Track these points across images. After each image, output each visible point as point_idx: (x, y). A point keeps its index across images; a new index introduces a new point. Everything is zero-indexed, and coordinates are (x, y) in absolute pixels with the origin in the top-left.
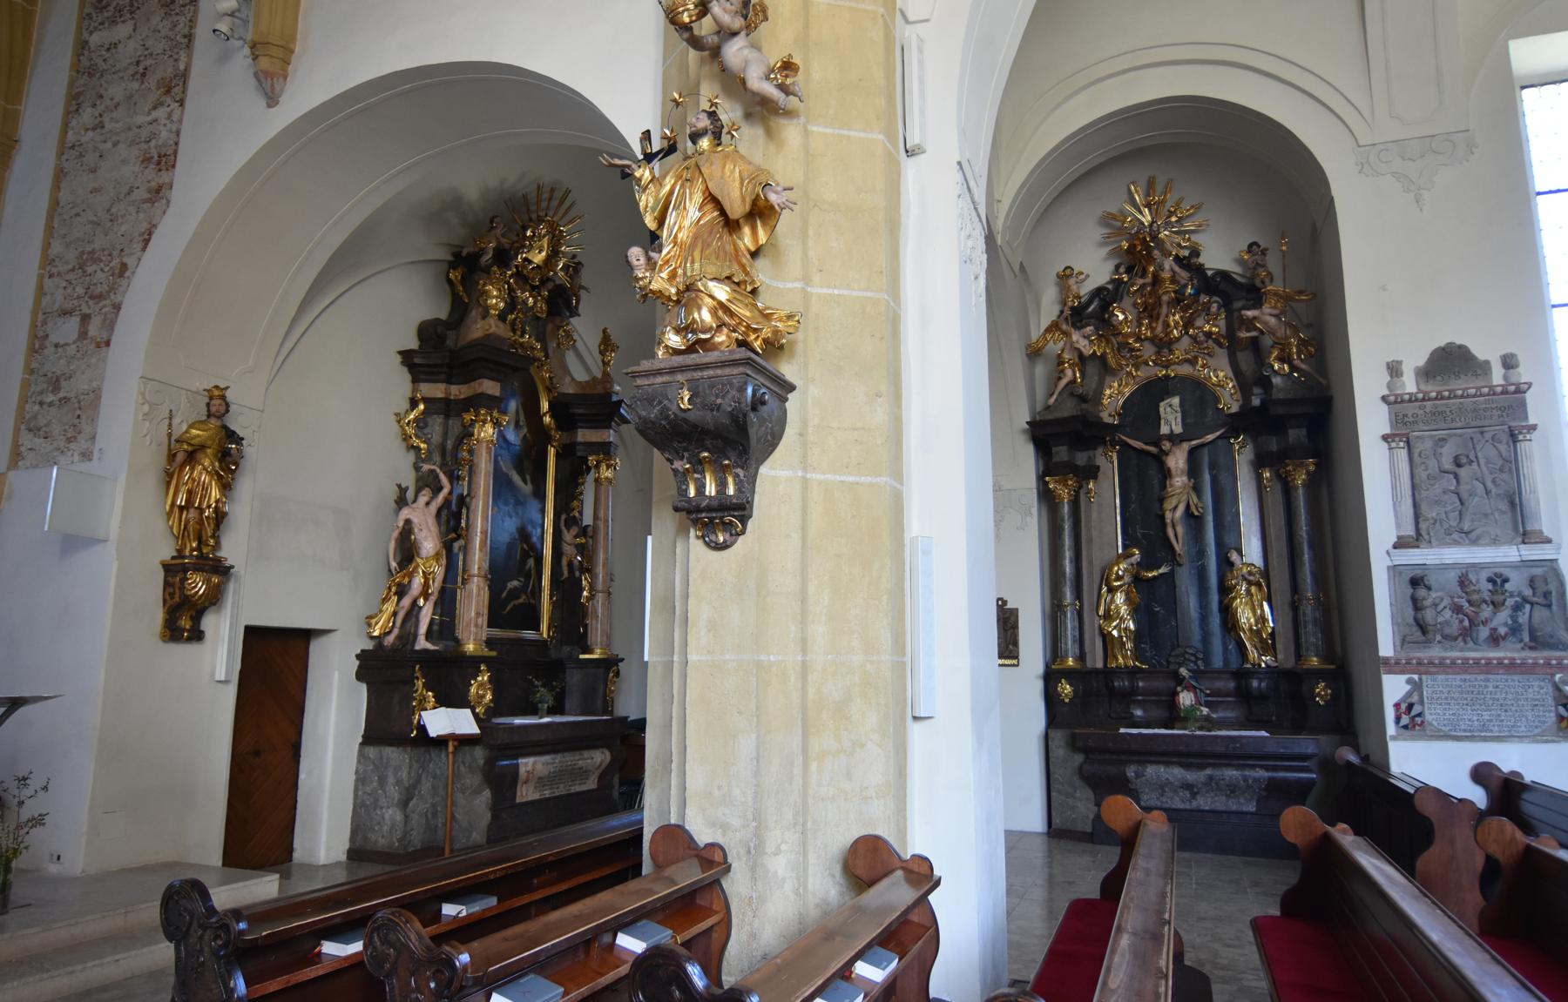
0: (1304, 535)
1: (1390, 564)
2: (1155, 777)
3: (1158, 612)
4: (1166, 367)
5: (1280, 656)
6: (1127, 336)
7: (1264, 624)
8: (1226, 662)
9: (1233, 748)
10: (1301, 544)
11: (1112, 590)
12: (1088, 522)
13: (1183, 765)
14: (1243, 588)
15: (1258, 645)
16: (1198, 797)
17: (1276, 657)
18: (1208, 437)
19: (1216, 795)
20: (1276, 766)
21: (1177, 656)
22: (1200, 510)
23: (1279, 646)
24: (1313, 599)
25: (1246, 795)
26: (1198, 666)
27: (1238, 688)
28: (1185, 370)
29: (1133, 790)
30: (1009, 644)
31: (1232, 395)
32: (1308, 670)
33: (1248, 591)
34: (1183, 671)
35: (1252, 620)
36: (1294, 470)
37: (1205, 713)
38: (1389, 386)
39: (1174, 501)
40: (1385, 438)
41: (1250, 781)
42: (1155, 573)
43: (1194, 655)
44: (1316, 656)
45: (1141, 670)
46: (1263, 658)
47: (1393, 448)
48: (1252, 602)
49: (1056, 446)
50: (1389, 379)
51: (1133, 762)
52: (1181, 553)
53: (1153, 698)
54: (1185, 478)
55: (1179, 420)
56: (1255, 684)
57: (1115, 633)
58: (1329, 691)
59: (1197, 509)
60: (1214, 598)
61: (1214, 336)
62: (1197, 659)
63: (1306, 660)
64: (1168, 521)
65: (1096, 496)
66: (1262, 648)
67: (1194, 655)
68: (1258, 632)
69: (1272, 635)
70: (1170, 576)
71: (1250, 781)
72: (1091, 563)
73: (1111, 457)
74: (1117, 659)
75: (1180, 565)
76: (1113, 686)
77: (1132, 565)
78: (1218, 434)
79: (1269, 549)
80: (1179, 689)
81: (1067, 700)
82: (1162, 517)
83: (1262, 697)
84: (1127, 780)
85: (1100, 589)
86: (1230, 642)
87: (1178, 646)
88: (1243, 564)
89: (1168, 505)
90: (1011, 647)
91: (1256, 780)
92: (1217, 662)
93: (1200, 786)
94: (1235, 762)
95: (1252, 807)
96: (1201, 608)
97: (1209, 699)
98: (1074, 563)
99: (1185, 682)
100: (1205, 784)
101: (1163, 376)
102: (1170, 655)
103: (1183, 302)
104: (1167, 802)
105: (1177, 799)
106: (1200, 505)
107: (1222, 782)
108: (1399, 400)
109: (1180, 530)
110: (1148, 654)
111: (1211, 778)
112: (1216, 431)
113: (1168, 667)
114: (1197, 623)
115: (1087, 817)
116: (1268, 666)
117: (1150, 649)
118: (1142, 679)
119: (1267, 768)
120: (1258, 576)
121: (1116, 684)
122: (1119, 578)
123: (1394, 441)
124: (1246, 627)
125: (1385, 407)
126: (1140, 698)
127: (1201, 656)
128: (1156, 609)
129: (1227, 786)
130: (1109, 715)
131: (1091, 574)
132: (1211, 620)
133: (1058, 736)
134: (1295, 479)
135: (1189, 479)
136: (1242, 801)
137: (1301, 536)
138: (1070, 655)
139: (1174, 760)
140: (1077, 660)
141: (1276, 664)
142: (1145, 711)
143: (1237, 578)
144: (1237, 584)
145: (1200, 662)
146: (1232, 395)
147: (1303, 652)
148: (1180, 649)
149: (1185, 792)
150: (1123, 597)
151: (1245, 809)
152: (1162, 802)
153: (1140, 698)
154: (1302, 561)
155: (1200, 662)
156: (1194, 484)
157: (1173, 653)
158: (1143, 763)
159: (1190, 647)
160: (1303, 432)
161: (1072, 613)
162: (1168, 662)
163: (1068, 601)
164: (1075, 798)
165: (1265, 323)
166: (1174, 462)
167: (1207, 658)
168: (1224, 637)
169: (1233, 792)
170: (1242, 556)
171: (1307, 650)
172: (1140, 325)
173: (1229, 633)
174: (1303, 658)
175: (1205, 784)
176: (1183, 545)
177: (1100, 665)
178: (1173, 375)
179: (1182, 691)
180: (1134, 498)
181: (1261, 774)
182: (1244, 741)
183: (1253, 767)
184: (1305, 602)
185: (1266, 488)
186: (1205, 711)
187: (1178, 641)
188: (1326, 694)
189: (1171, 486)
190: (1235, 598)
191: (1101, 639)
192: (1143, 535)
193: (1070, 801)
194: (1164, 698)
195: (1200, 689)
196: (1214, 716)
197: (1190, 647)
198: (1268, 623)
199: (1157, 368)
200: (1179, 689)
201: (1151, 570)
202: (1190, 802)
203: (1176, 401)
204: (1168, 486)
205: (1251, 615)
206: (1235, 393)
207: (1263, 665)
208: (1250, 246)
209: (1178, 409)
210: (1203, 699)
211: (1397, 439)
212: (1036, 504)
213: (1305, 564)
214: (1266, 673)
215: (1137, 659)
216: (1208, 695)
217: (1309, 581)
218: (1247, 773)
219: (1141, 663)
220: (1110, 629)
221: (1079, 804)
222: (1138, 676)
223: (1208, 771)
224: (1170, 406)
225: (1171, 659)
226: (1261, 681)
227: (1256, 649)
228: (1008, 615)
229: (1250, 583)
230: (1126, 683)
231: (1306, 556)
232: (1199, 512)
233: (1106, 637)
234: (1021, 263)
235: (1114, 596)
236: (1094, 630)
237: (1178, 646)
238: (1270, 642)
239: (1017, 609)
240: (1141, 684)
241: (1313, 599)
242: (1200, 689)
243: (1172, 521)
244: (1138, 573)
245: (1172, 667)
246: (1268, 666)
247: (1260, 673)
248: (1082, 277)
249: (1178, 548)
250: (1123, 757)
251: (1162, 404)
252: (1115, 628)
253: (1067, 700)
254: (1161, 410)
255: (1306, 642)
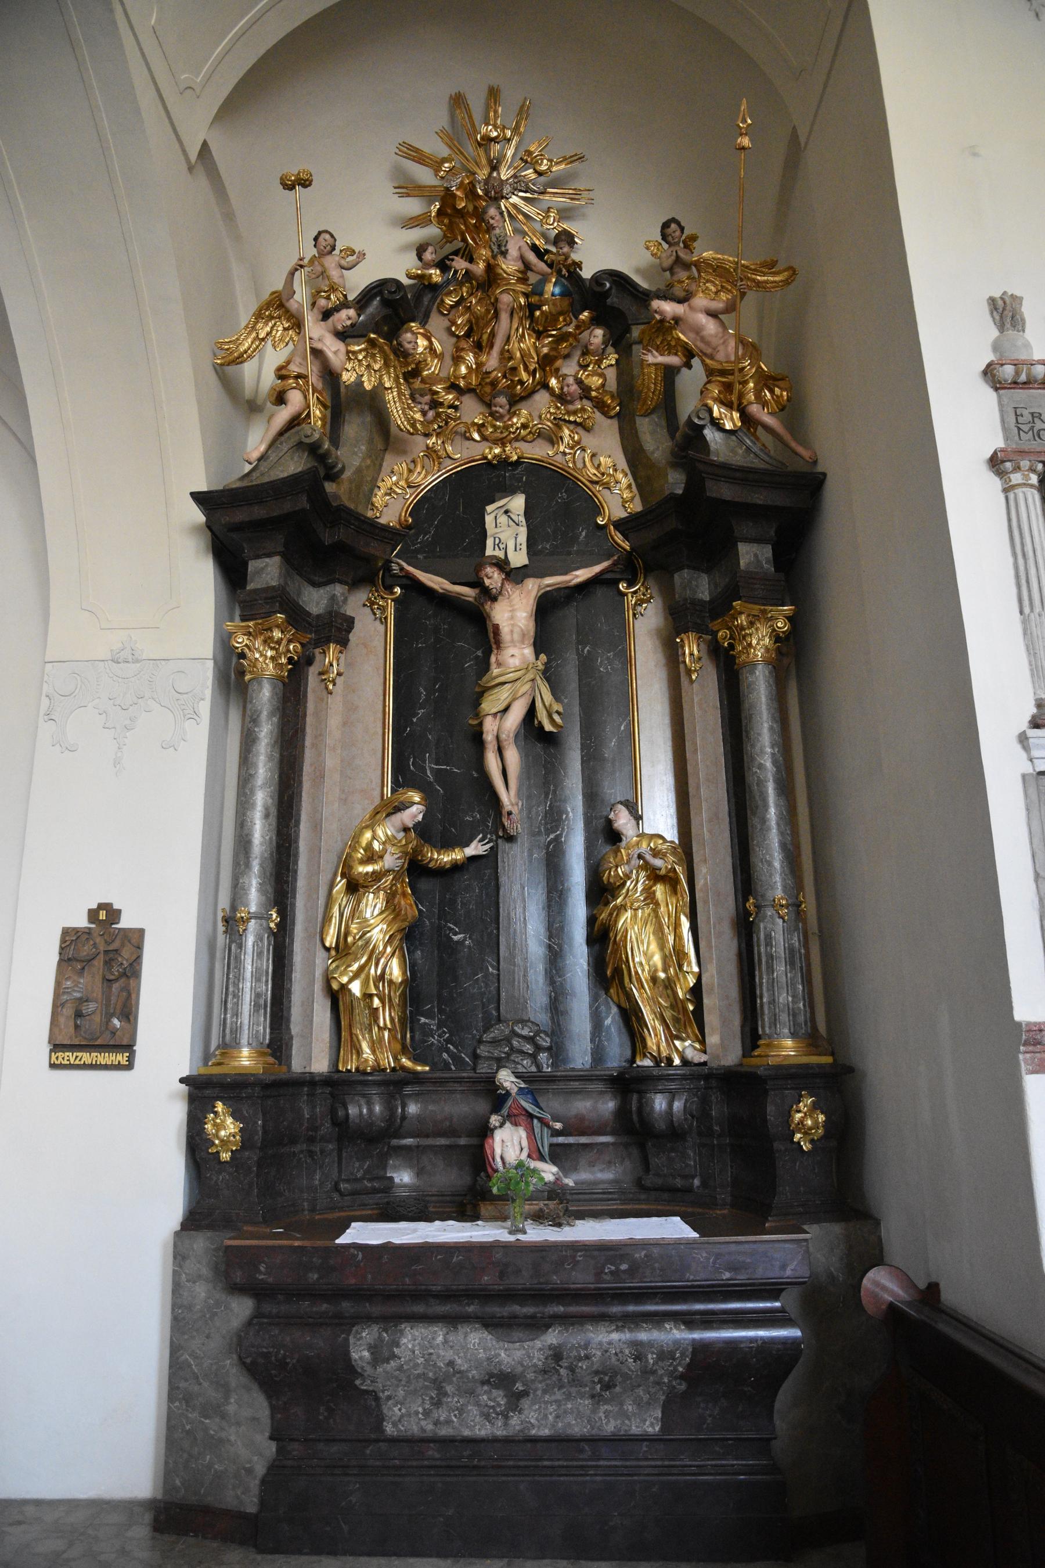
0: (769, 764)
1: (1028, 769)
2: (421, 1360)
3: (461, 943)
4: (502, 442)
5: (713, 1039)
6: (434, 379)
7: (680, 966)
8: (598, 1055)
9: (612, 1273)
10: (761, 783)
11: (354, 887)
12: (319, 736)
13: (490, 1324)
14: (640, 887)
15: (668, 1015)
16: (525, 1403)
17: (703, 1042)
18: (578, 573)
19: (569, 1397)
20: (713, 1312)
21: (495, 1042)
22: (556, 717)
23: (711, 1019)
24: (787, 906)
25: (640, 1391)
26: (539, 1067)
27: (622, 1113)
28: (538, 451)
29: (367, 1392)
30: (113, 1015)
31: (624, 501)
32: (778, 1067)
33: (650, 896)
34: (506, 1078)
35: (657, 959)
36: (751, 624)
37: (549, 1177)
38: (996, 347)
39: (503, 695)
40: (995, 462)
41: (651, 1358)
42: (456, 855)
43: (530, 1040)
44: (794, 1035)
45: (416, 1078)
46: (677, 1043)
47: (1013, 487)
48: (657, 916)
49: (258, 557)
50: (995, 333)
51: (369, 1319)
52: (515, 810)
53: (442, 1141)
54: (528, 652)
55: (523, 538)
56: (659, 1103)
57: (356, 988)
58: (821, 1118)
59: (550, 716)
60: (578, 910)
61: (594, 394)
62: (538, 1049)
63: (769, 1046)
64: (489, 737)
65: (340, 681)
66: (676, 1020)
67: (530, 1040)
68: (669, 985)
69: (696, 991)
70: (488, 863)
71: (651, 1358)
72: (317, 827)
73: (383, 609)
74: (359, 1052)
75: (510, 839)
76: (347, 1115)
77: (406, 830)
78: (597, 569)
79: (693, 802)
80: (494, 1120)
81: (225, 1156)
82: (477, 738)
83: (674, 1134)
84: (352, 1370)
85: (332, 885)
86: (609, 1008)
87: (499, 1020)
88: (642, 835)
89: (490, 704)
90: (116, 1022)
91: (665, 1355)
92: (580, 1056)
93: (530, 1376)
94: (616, 1309)
95: (650, 1424)
96: (550, 938)
97: (561, 1140)
98: (273, 820)
99: (510, 1102)
100: (545, 1372)
101: (495, 456)
102: (480, 1042)
103: (539, 308)
104: (448, 1422)
105: (473, 1410)
106: (557, 707)
107: (584, 1365)
108: (1023, 378)
109: (513, 756)
110: (433, 1040)
111: (557, 1355)
112: (599, 563)
113: (474, 1069)
114: (541, 967)
115: (250, 1471)
116: (685, 1062)
117: (439, 1027)
118: (416, 1096)
119: (689, 1321)
120: (671, 858)
121: (353, 1111)
122: (371, 857)
123: (1017, 468)
124: (644, 976)
125: (990, 396)
126: (409, 1141)
127: (545, 1041)
128: (456, 938)
129: (597, 1372)
130: (336, 1188)
131: (316, 850)
132: (569, 960)
133: (201, 1243)
134: (750, 645)
135: (538, 651)
136: (629, 1408)
137: (761, 766)
138: (244, 1041)
139: (471, 1309)
140: (261, 1054)
141: (703, 1058)
142: (419, 1173)
143: (628, 862)
144: (628, 876)
145: (543, 1056)
146: (624, 501)
147: (765, 1027)
148: (502, 1026)
149: (495, 1393)
150: (380, 904)
151: (635, 1430)
152: (437, 1423)
153: (409, 1141)
154: (764, 821)
155: (543, 1056)
156: (546, 664)
157: (486, 1037)
158: (393, 1320)
159: (524, 1022)
160: (766, 552)
161: (259, 938)
162: (476, 1057)
163: (253, 909)
164: (223, 1416)
165: (698, 330)
166: (507, 615)
167: (557, 1051)
168: (594, 999)
169: (608, 1387)
170: (638, 818)
171: (774, 1022)
172: (457, 360)
173: (607, 991)
174: (761, 1042)
175: (545, 1372)
176: (519, 794)
177: (320, 1065)
178: (515, 458)
179: (501, 1126)
180: (423, 697)
181: (678, 1335)
182: (639, 1255)
183: (657, 1319)
184: (769, 912)
185: (689, 672)
186: (549, 1171)
187: (498, 1009)
188: (816, 1126)
189: (499, 665)
190: (623, 908)
191: (328, 1004)
192: (437, 773)
193: (212, 1424)
194: (463, 1141)
195: (540, 1119)
196: (569, 1182)
197: (524, 1022)
198: (689, 964)
199: (486, 444)
200: (494, 1120)
201: (447, 844)
202: (506, 1417)
203: (518, 503)
204: (493, 666)
205: (654, 947)
206: (632, 499)
207: (677, 1061)
208: (665, 226)
209: (522, 519)
210: (547, 1141)
211: (1025, 464)
212: (208, 693)
213: (769, 829)
214: (684, 1077)
215: (404, 1050)
216: (557, 1133)
217: (777, 864)
218: (643, 1336)
219: (416, 1059)
220: (345, 980)
221: (232, 1434)
222: (408, 1090)
223: (552, 1337)
224: (506, 512)
225: (483, 1051)
226: (672, 1095)
227: (663, 1021)
228: (115, 945)
229: (655, 876)
230: (377, 1108)
231: (772, 811)
232: (552, 721)
233: (336, 997)
234: (205, 144)
235: (359, 902)
236: (312, 982)
237: (499, 1020)
238: (691, 1008)
239: (141, 932)
240: (413, 1109)
241: (787, 906)
242: (540, 1119)
243: (498, 738)
244: (416, 851)
245: (483, 1068)
246: (685, 1062)
247: (668, 1078)
248: (354, 258)
249: (508, 798)
250: (346, 1306)
251: (489, 508)
252: (356, 975)
253: (225, 1156)
254: (489, 520)
255: (773, 1002)
